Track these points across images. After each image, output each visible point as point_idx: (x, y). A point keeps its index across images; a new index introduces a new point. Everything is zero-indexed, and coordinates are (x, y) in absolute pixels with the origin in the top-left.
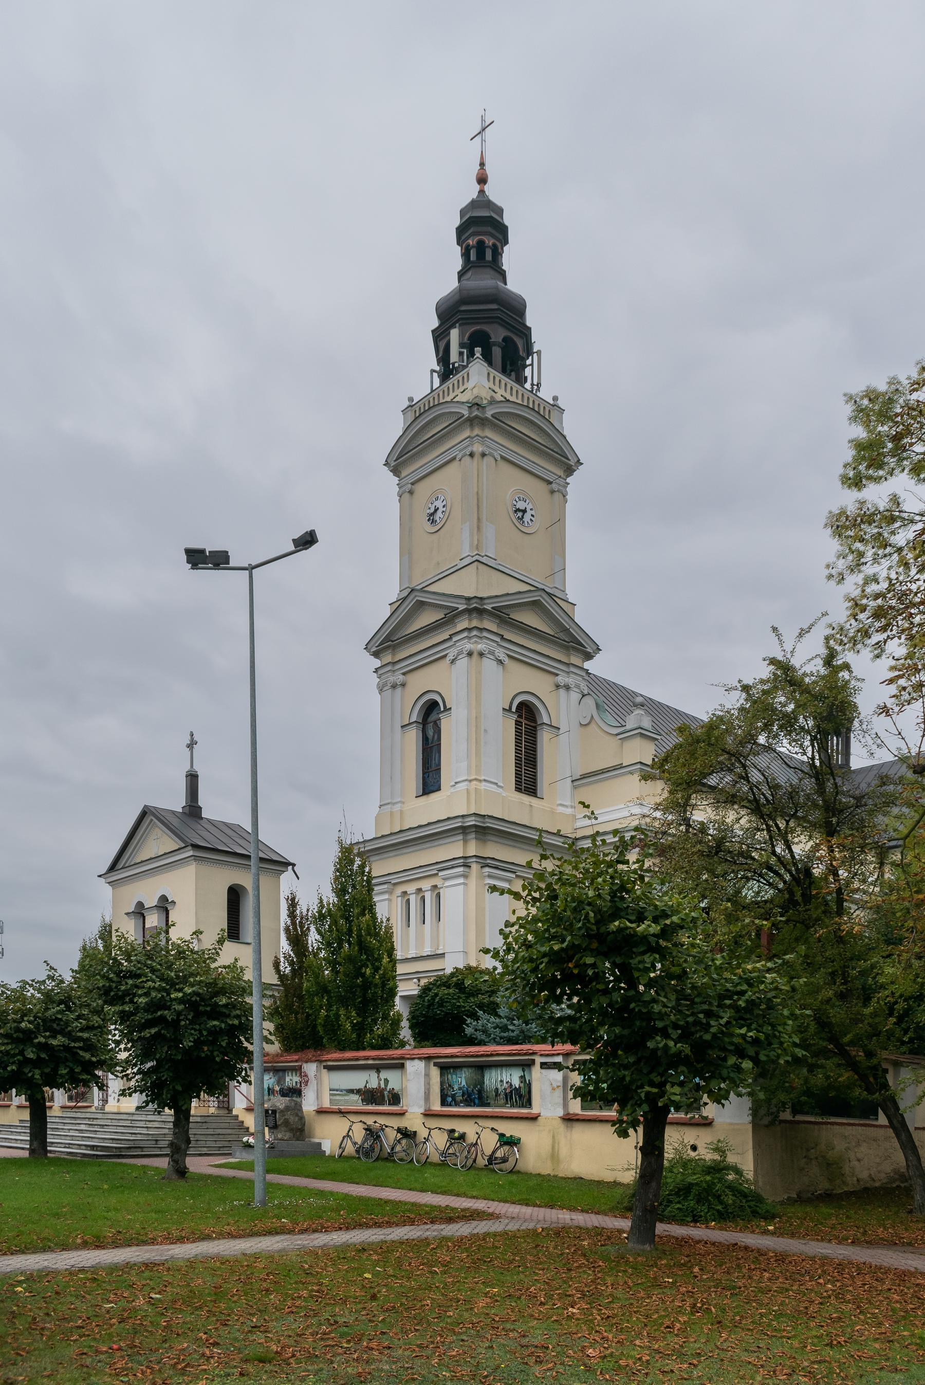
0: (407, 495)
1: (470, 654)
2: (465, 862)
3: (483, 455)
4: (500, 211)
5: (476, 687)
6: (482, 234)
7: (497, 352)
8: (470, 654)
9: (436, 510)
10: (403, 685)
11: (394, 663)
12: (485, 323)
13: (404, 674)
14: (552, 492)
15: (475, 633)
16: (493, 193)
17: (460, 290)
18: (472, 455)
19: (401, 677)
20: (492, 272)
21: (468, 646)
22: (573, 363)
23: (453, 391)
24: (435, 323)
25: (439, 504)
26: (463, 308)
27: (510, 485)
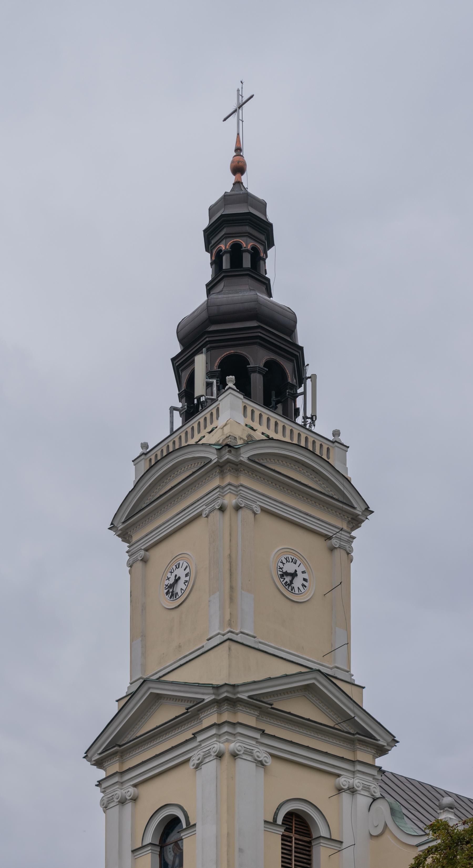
0: (139, 565)
1: (220, 756)
3: (238, 508)
4: (262, 205)
6: (239, 235)
7: (257, 381)
8: (220, 756)
9: (177, 580)
10: (134, 799)
11: (122, 773)
12: (243, 345)
13: (135, 786)
14: (332, 549)
15: (225, 729)
16: (253, 184)
17: (208, 305)
18: (222, 509)
19: (132, 790)
24: (177, 349)
25: (180, 572)
26: (213, 328)
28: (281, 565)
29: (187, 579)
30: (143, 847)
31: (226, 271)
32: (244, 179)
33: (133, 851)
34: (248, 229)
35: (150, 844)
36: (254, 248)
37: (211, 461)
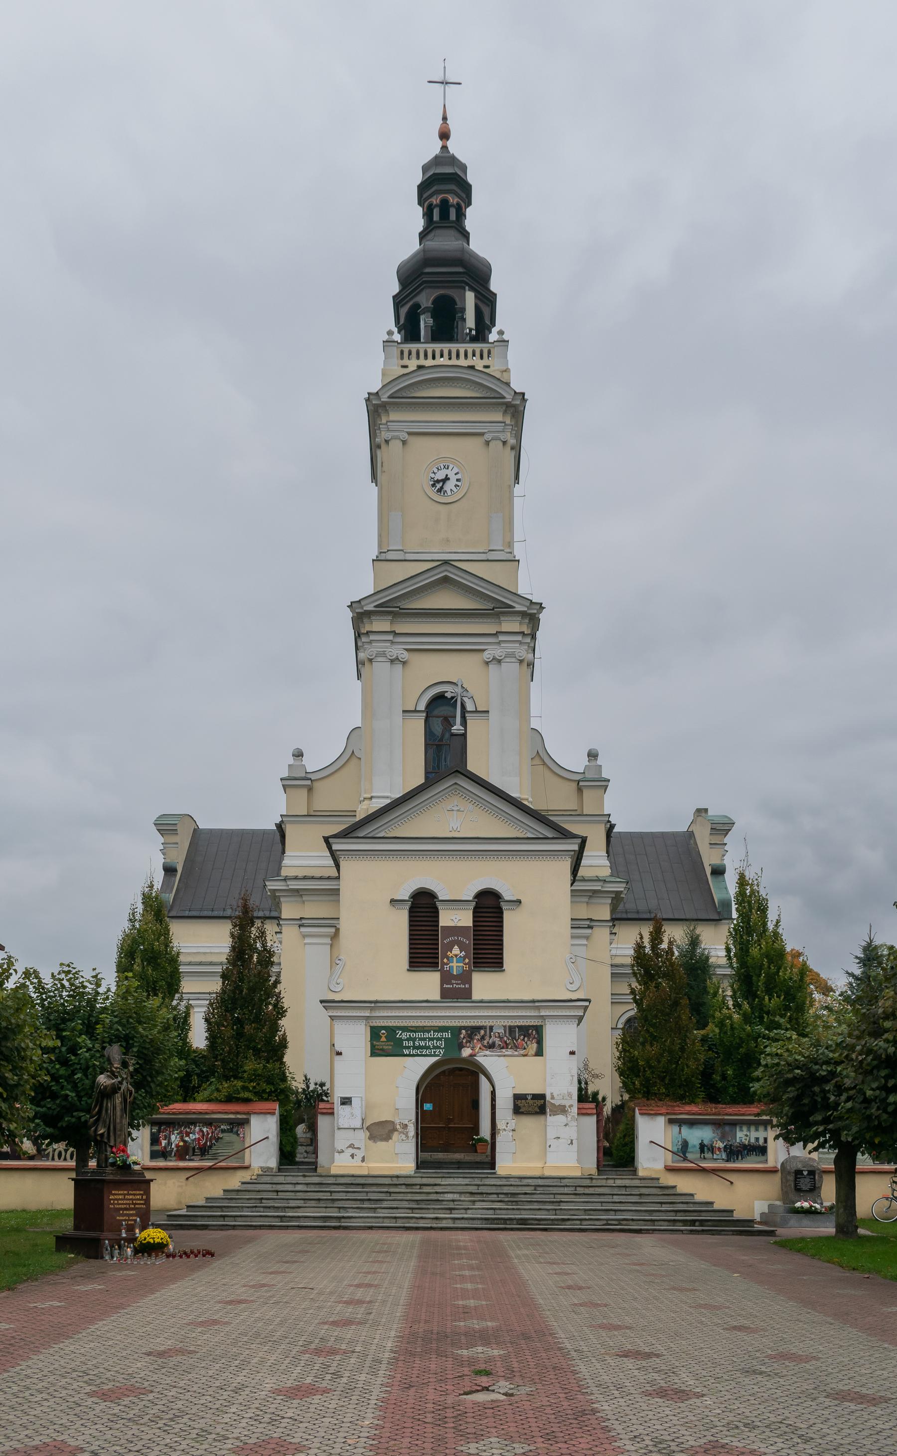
1: (521, 661)
4: (464, 168)
6: (445, 191)
8: (521, 661)
9: (447, 479)
10: (404, 663)
13: (406, 650)
16: (453, 147)
17: (424, 251)
18: (504, 443)
26: (428, 270)
28: (433, 475)
30: (416, 711)
31: (436, 222)
33: (404, 711)
34: (453, 187)
36: (458, 204)
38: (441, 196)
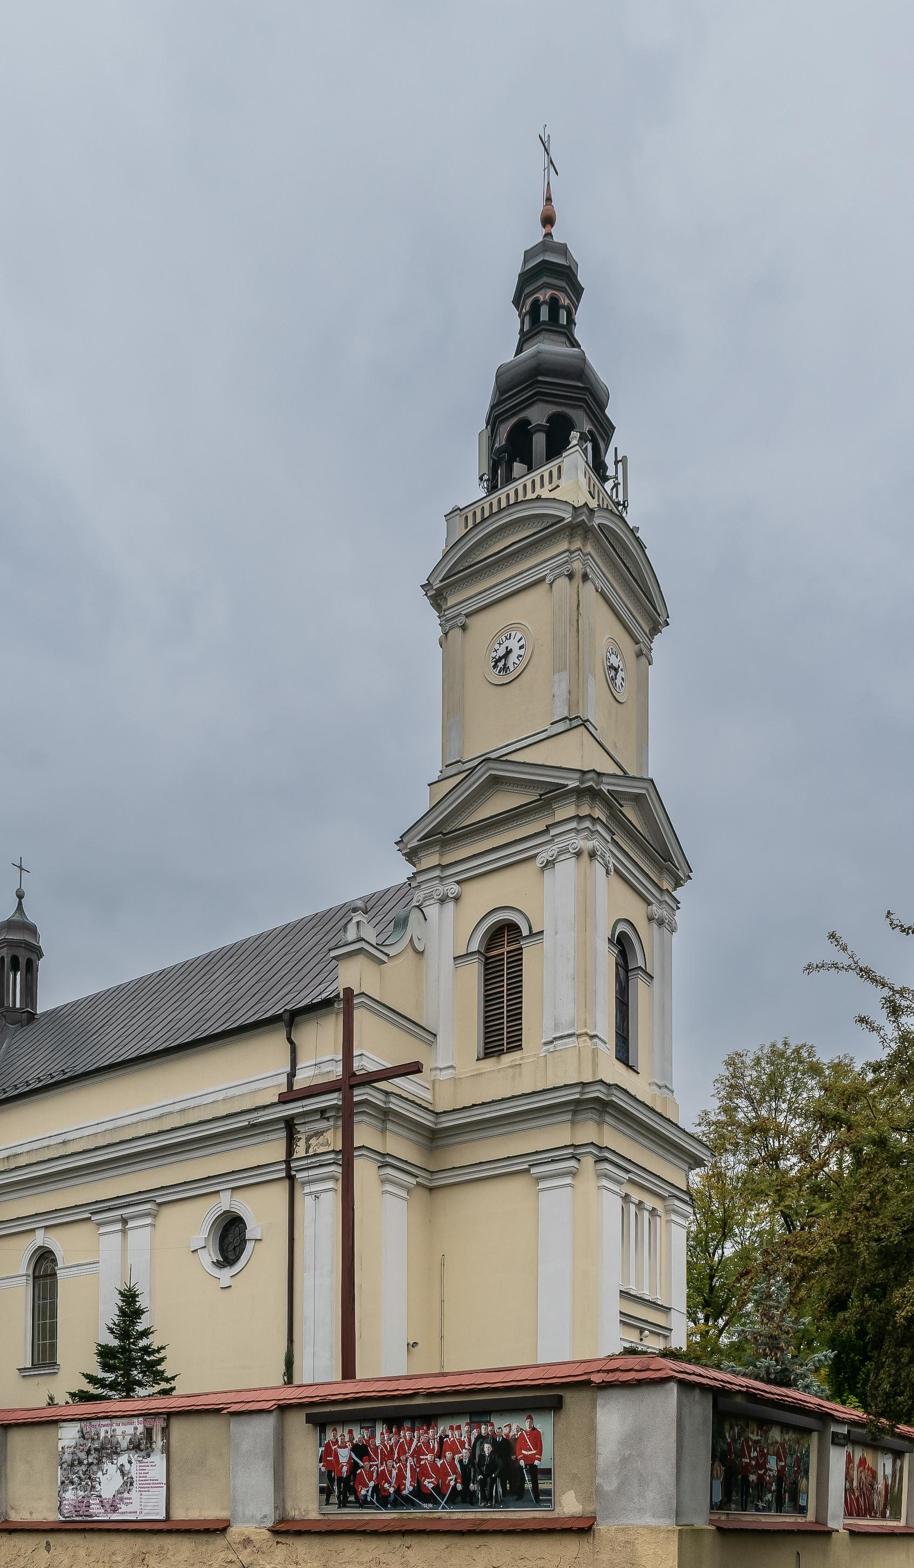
0: (457, 632)
1: (578, 854)
2: (574, 1152)
5: (567, 899)
6: (548, 289)
8: (578, 854)
9: (509, 652)
10: (457, 899)
11: (444, 867)
12: (546, 407)
13: (458, 882)
15: (587, 824)
18: (571, 576)
19: (456, 887)
20: (564, 339)
21: (581, 842)
22: (663, 464)
23: (533, 491)
25: (513, 644)
27: (604, 631)
29: (522, 652)
31: (544, 322)
32: (553, 231)
35: (478, 952)
37: (563, 519)
38: (549, 293)
